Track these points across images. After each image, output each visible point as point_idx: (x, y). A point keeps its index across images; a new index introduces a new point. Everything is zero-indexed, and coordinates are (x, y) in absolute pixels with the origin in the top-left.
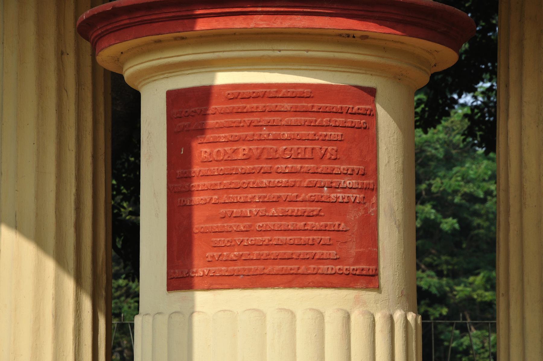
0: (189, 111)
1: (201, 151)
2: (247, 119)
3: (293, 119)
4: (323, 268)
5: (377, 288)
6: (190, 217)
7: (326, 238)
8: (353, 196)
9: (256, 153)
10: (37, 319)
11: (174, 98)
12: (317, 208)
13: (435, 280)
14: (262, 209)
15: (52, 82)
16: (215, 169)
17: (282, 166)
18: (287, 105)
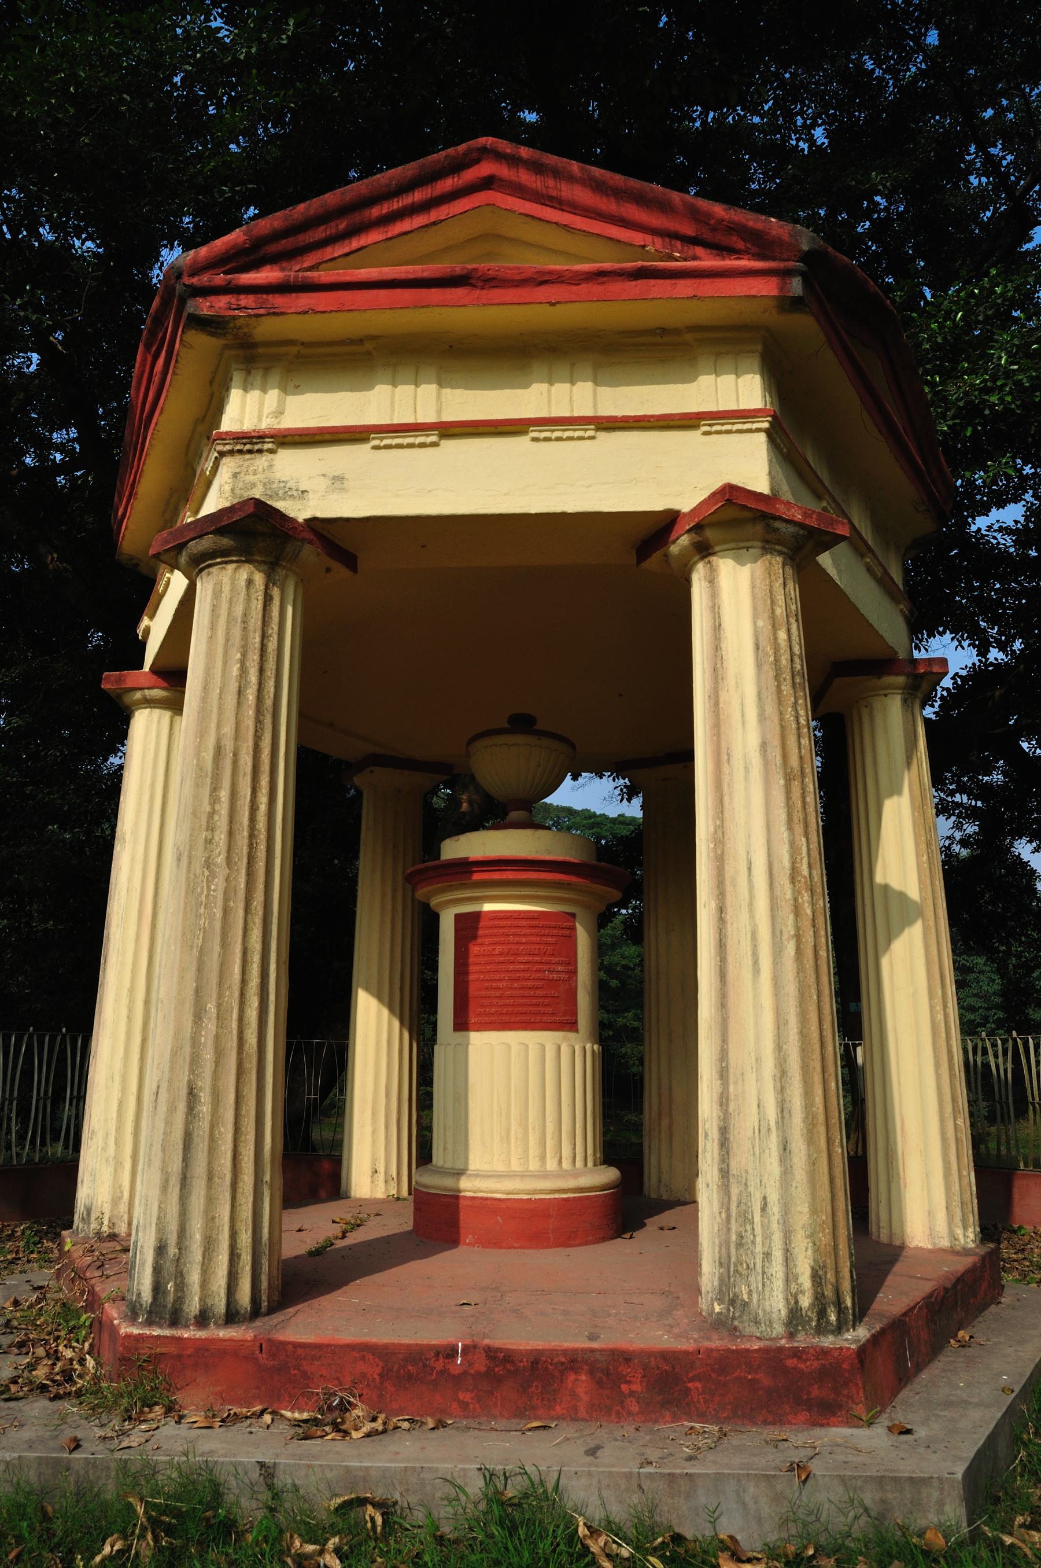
0: (469, 926)
1: (475, 949)
2: (501, 931)
3: (528, 931)
4: (545, 1019)
5: (577, 1031)
6: (467, 988)
7: (546, 1001)
8: (563, 976)
9: (506, 951)
10: (378, 1043)
11: (458, 917)
12: (541, 983)
13: (606, 1015)
14: (509, 984)
15: (389, 907)
16: (482, 960)
17: (521, 959)
18: (524, 923)
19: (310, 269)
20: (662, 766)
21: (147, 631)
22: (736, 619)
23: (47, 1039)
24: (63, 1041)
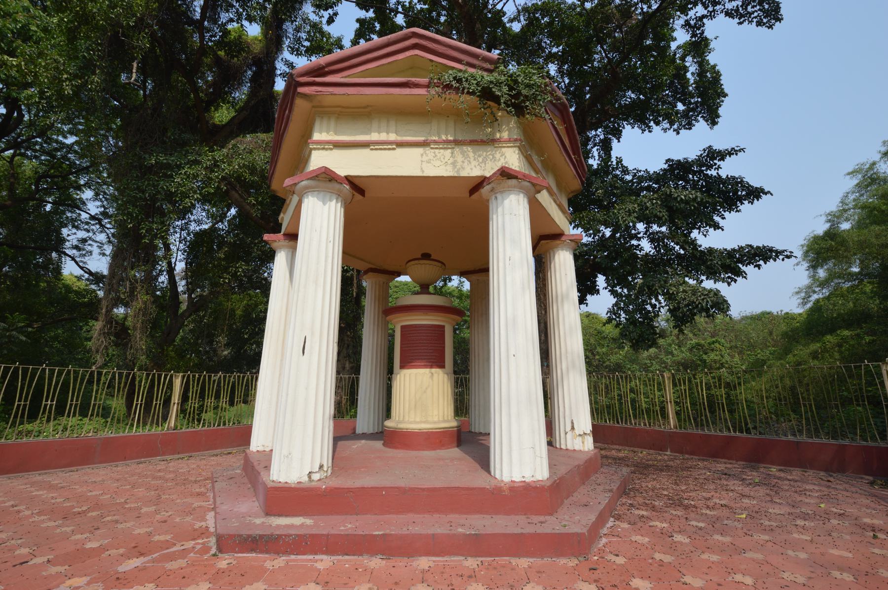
11: (403, 327)
19: (346, 77)
20: (479, 271)
21: (283, 218)
23: (178, 383)
24: (204, 379)
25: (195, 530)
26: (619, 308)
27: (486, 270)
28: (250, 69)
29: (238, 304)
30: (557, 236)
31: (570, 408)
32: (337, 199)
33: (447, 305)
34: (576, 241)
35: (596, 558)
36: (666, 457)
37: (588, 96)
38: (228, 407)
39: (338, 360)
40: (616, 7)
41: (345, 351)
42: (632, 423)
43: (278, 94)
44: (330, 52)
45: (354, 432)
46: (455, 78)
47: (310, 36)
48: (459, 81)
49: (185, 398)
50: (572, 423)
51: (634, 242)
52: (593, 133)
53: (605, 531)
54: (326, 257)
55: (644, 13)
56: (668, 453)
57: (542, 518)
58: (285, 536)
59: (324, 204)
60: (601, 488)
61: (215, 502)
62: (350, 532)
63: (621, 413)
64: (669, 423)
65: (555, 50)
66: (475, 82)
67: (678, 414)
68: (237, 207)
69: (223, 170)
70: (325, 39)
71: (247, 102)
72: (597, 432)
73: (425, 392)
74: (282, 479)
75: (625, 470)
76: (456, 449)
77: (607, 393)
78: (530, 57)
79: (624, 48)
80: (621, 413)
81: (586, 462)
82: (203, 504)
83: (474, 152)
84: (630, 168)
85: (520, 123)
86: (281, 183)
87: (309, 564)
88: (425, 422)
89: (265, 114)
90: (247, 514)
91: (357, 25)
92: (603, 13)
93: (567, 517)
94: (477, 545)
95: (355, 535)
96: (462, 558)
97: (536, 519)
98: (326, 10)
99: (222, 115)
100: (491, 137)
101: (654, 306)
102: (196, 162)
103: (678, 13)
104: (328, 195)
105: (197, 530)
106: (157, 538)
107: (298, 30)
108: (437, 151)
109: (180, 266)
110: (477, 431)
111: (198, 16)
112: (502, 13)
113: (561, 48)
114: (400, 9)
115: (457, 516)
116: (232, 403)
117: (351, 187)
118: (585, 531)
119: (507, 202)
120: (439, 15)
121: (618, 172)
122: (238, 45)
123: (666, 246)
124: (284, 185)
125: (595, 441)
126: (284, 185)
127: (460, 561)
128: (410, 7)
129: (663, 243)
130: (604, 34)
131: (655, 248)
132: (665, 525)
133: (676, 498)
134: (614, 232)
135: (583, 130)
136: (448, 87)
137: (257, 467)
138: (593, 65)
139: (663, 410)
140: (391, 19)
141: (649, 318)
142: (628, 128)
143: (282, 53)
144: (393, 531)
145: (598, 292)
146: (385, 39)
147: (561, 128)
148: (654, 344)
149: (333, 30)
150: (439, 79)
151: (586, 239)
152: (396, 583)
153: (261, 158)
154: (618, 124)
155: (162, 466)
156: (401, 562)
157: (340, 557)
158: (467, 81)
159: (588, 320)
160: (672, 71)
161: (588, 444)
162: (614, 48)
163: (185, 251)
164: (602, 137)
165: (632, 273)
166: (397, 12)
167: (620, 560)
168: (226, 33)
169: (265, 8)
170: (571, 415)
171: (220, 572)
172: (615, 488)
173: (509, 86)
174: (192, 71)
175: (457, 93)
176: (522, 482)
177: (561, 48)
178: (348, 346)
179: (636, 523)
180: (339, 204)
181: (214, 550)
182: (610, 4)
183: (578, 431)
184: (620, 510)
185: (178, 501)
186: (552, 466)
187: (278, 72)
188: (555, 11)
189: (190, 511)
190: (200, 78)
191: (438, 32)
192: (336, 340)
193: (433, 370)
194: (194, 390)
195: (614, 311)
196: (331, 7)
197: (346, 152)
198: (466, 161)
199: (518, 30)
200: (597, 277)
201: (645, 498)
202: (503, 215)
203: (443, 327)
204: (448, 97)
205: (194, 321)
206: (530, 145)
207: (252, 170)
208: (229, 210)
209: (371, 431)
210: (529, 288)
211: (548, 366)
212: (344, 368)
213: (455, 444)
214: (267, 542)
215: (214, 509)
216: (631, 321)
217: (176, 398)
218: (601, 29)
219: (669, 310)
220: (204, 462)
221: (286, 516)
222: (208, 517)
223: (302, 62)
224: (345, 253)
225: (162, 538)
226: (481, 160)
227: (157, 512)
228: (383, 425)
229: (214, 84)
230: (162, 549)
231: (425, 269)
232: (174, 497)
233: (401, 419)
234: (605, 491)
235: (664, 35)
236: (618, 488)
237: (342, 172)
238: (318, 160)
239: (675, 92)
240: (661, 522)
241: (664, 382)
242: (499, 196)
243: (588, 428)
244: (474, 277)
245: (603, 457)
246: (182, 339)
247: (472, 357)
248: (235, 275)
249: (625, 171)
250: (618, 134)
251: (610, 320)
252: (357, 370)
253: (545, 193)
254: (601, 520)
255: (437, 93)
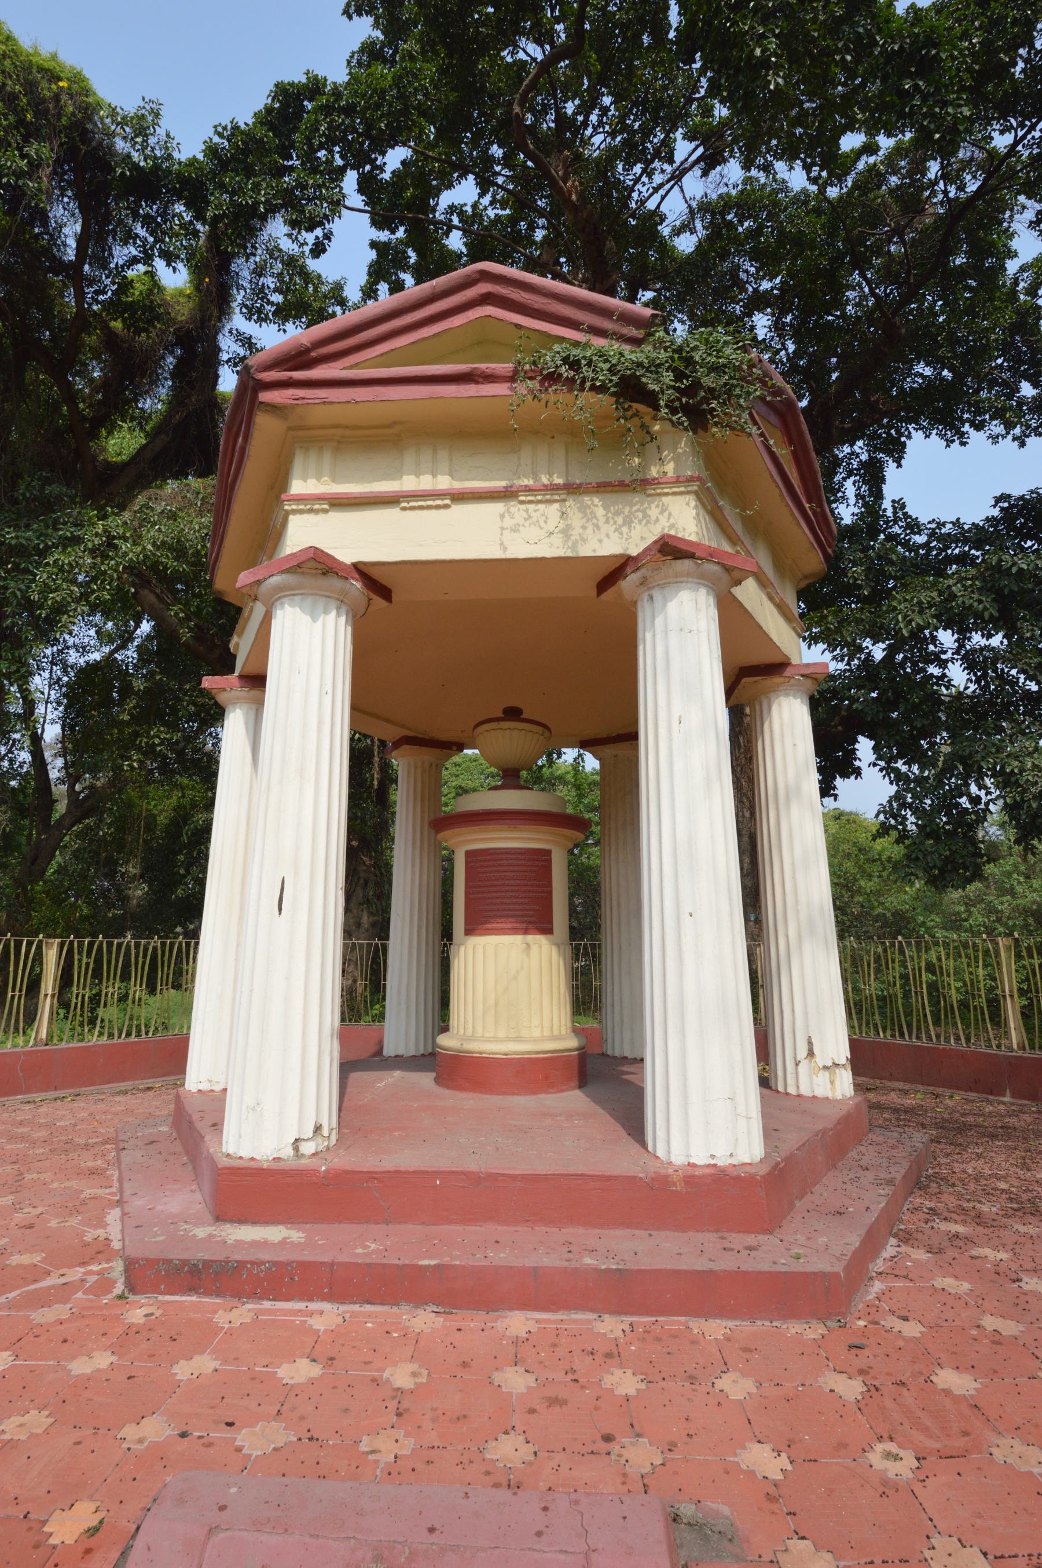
11: (468, 854)
19: (351, 367)
20: (619, 737)
21: (237, 645)
22: (680, 653)
23: (51, 956)
25: (86, 1245)
26: (904, 805)
27: (632, 737)
28: (172, 353)
29: (162, 805)
30: (775, 668)
31: (806, 1013)
32: (338, 609)
33: (555, 809)
34: (810, 674)
35: (862, 1323)
36: (1002, 1107)
37: (834, 376)
38: (145, 997)
39: (347, 910)
40: (891, 191)
41: (359, 892)
42: (932, 1038)
43: (225, 400)
44: (322, 316)
45: (379, 1052)
46: (565, 360)
47: (282, 282)
48: (574, 364)
49: (65, 980)
50: (810, 1043)
51: (934, 670)
52: (847, 449)
53: (879, 1265)
54: (320, 723)
55: (949, 199)
56: (1007, 1099)
57: (750, 1239)
58: (252, 1263)
59: (314, 619)
60: (870, 1176)
61: (121, 1190)
62: (374, 1259)
63: (908, 1014)
64: (1007, 1034)
65: (766, 285)
66: (608, 365)
67: (1026, 1014)
68: (152, 618)
69: (125, 554)
70: (311, 289)
71: (167, 417)
72: (863, 1059)
73: (515, 978)
74: (245, 1153)
75: (919, 1138)
76: (578, 1093)
77: (878, 971)
78: (714, 301)
79: (908, 274)
80: (908, 1014)
81: (839, 1122)
82: (101, 1192)
83: (606, 507)
84: (923, 520)
85: (699, 444)
86: (233, 579)
87: (298, 1320)
88: (517, 1039)
89: (200, 440)
90: (180, 1217)
91: (373, 255)
92: (864, 205)
93: (801, 1239)
94: (625, 1291)
95: (384, 1266)
96: (592, 1316)
97: (739, 1240)
98: (310, 229)
99: (122, 443)
100: (640, 476)
101: (975, 800)
102: (76, 540)
103: (1022, 198)
104: (321, 602)
105: (88, 1244)
106: (16, 1260)
107: (259, 271)
108: (531, 507)
109: (52, 732)
110: (617, 1054)
111: (71, 255)
112: (657, 216)
113: (778, 280)
114: (455, 220)
115: (581, 1230)
116: (152, 990)
117: (365, 585)
118: (838, 1268)
119: (672, 607)
120: (532, 227)
121: (896, 529)
122: (146, 309)
123: (1001, 677)
124: (238, 585)
125: (856, 1073)
126: (238, 585)
127: (589, 1322)
128: (474, 215)
129: (995, 671)
130: (866, 247)
131: (978, 681)
132: (1003, 1255)
133: (1025, 1197)
134: (891, 652)
135: (826, 443)
136: (553, 378)
137: (199, 1125)
138: (844, 313)
139: (995, 1006)
140: (438, 241)
141: (968, 823)
142: (918, 436)
143: (230, 319)
144: (456, 1258)
145: (858, 772)
146: (428, 286)
147: (783, 453)
148: (977, 875)
149: (326, 268)
150: (534, 363)
151: (835, 667)
152: (465, 1365)
153: (195, 526)
154: (898, 432)
155: (25, 1113)
156: (473, 1321)
157: (356, 1307)
158: (589, 364)
159: (840, 829)
160: (1009, 317)
161: (843, 1086)
162: (888, 275)
163: (59, 703)
164: (864, 457)
165: (929, 732)
166: (451, 227)
167: (912, 1329)
168: (125, 286)
169: (196, 233)
170: (807, 1026)
171: (132, 1332)
172: (899, 1177)
173: (675, 370)
174: (63, 362)
175: (570, 390)
176: (709, 1166)
177: (778, 280)
178: (366, 882)
179: (948, 1251)
180: (343, 619)
181: (119, 1288)
182: (879, 187)
183: (820, 1060)
184: (909, 1221)
185: (55, 1185)
186: (770, 1133)
187: (225, 357)
188: (765, 207)
189: (75, 1206)
190: (78, 374)
191: (532, 265)
192: (342, 882)
193: (530, 938)
194: (83, 962)
195: (893, 810)
196: (321, 224)
197: (346, 516)
198: (589, 525)
199: (691, 249)
200: (856, 741)
201: (960, 1196)
202: (666, 632)
203: (548, 853)
204: (552, 398)
205: (79, 835)
206: (719, 487)
207: (179, 550)
208: (138, 626)
209: (412, 1052)
210: (720, 779)
211: (758, 921)
212: (359, 925)
213: (576, 1083)
214: (217, 1274)
215: (120, 1203)
216: (928, 830)
217: (49, 984)
218: (862, 238)
219: (1006, 807)
220: (102, 1106)
221: (254, 1222)
222: (109, 1219)
223: (273, 337)
224: (355, 708)
225: (26, 1259)
226: (620, 520)
227: (16, 1207)
228: (434, 1043)
229: (105, 385)
230: (26, 1281)
231: (512, 741)
232: (47, 1176)
233: (469, 1032)
234: (878, 1183)
235: (993, 244)
236: (904, 1177)
237: (347, 556)
238: (301, 533)
239: (1016, 360)
240: (995, 1248)
241: (997, 954)
242: (657, 594)
243: (842, 1052)
244: (609, 751)
245: (872, 1106)
246: (61, 870)
247: (606, 910)
248: (150, 751)
249: (914, 526)
250: (897, 450)
251: (884, 830)
252: (382, 929)
253: (750, 583)
254: (871, 1245)
255: (531, 391)
